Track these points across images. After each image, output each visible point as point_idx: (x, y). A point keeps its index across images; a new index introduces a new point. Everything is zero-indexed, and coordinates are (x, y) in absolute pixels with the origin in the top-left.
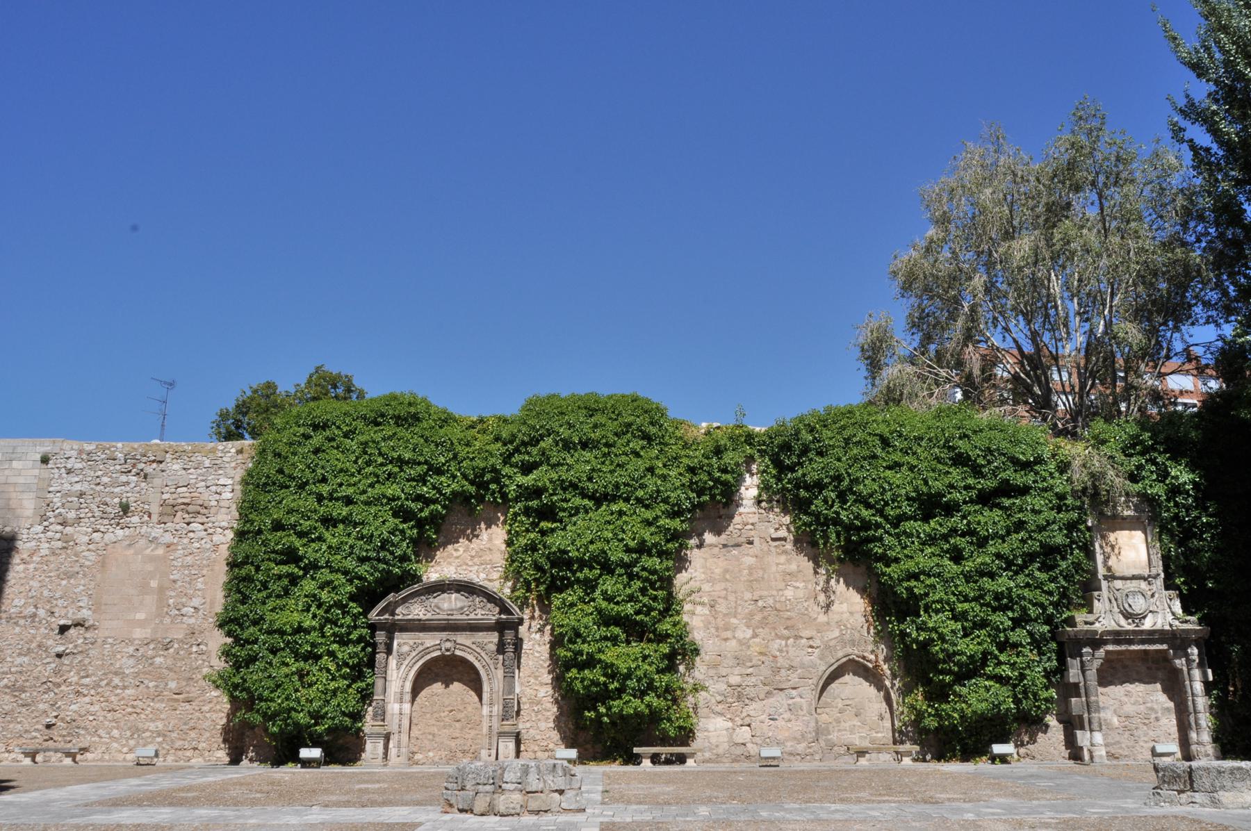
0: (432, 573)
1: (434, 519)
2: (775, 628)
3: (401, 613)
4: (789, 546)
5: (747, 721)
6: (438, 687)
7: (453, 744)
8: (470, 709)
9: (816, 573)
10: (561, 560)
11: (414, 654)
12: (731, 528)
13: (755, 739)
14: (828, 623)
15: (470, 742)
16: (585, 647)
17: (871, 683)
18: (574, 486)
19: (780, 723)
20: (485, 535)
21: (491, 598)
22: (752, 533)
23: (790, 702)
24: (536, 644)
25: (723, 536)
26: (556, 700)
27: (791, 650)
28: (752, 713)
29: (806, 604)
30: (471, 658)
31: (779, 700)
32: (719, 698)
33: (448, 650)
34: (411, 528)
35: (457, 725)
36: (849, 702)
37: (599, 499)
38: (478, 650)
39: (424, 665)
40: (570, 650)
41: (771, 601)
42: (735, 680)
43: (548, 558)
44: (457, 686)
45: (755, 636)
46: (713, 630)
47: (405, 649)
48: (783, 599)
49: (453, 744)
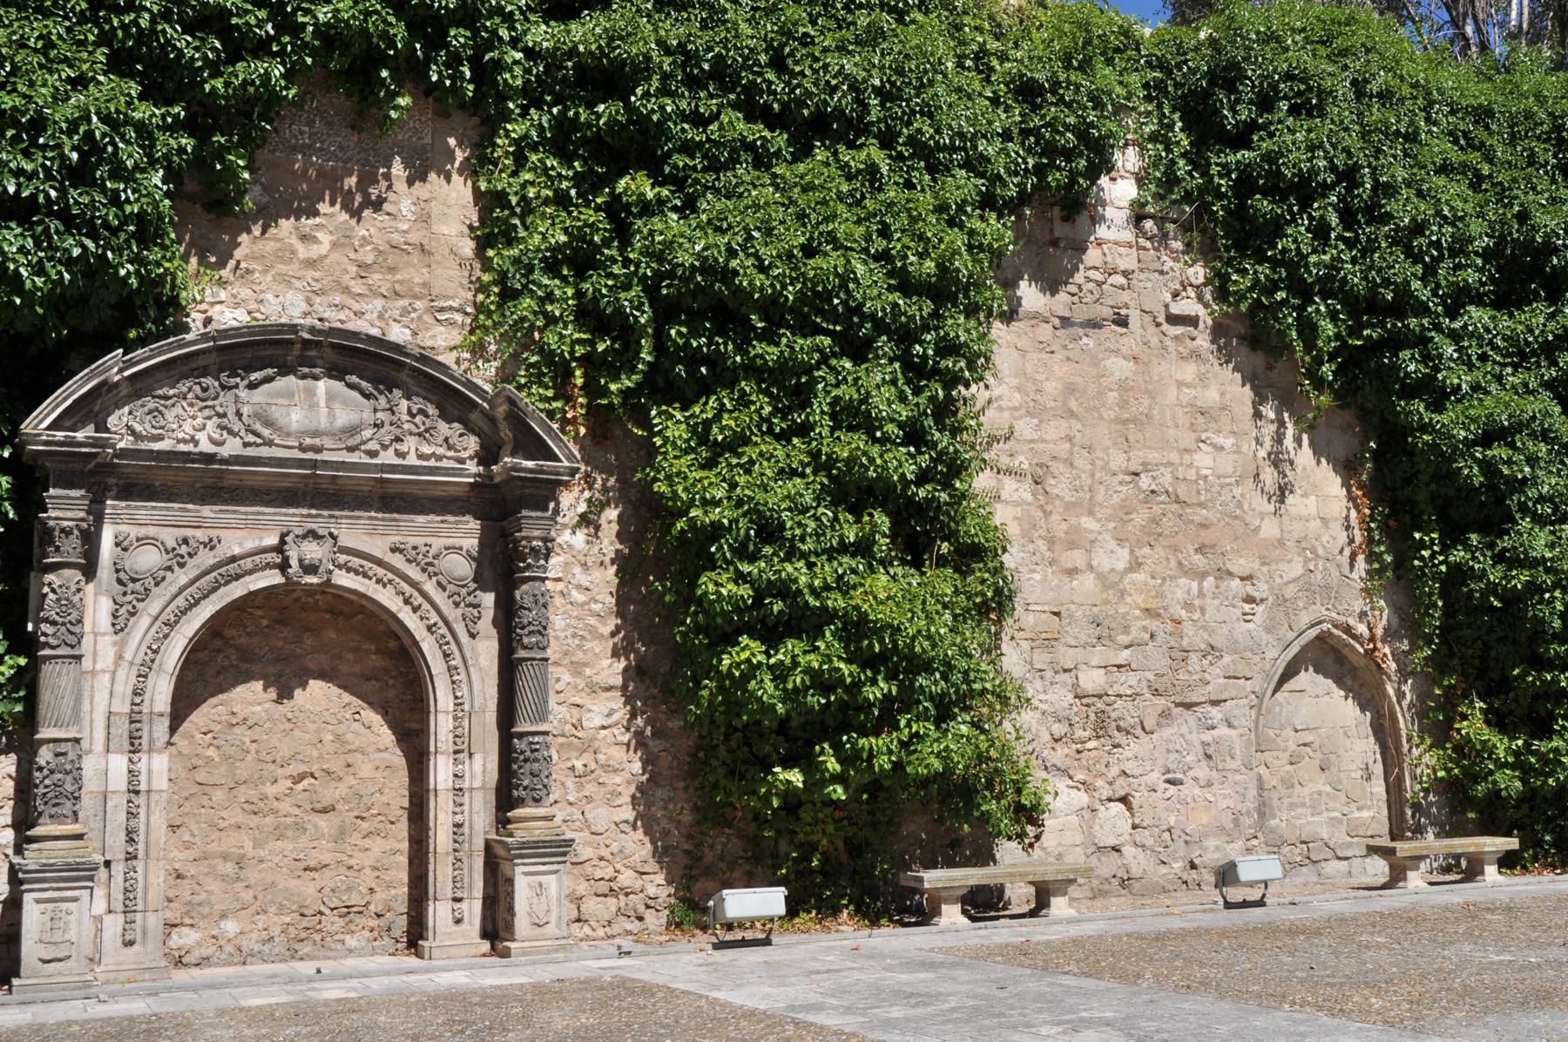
0: (220, 305)
1: (256, 107)
2: (1176, 549)
3: (125, 427)
4: (1203, 342)
5: (1121, 788)
6: (251, 697)
7: (307, 889)
8: (366, 770)
9: (1258, 415)
10: (711, 301)
11: (182, 577)
12: (1079, 277)
13: (1142, 836)
14: (1281, 542)
15: (368, 878)
16: (797, 572)
17: (1348, 689)
18: (723, 76)
19: (1189, 790)
20: (404, 199)
21: (452, 401)
22: (1126, 296)
23: (1208, 736)
24: (580, 569)
25: (1062, 296)
26: (639, 734)
27: (1211, 604)
28: (1130, 767)
29: (1237, 491)
30: (388, 599)
31: (1184, 727)
32: (1059, 729)
33: (311, 569)
34: (173, 128)
35: (323, 822)
36: (1308, 738)
37: (812, 128)
38: (413, 572)
39: (214, 630)
40: (740, 578)
41: (1167, 479)
42: (1092, 680)
43: (651, 290)
44: (319, 696)
45: (1135, 565)
46: (1042, 546)
47: (147, 559)
48: (1191, 475)
49: (307, 889)
